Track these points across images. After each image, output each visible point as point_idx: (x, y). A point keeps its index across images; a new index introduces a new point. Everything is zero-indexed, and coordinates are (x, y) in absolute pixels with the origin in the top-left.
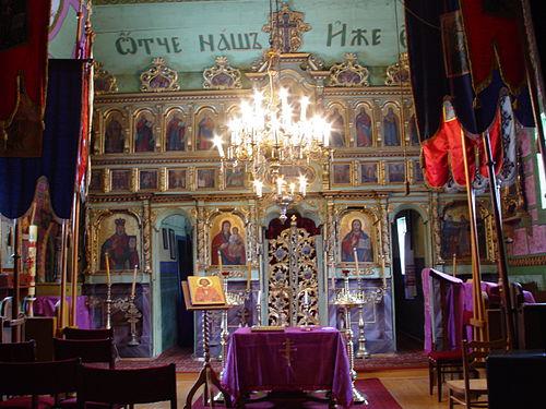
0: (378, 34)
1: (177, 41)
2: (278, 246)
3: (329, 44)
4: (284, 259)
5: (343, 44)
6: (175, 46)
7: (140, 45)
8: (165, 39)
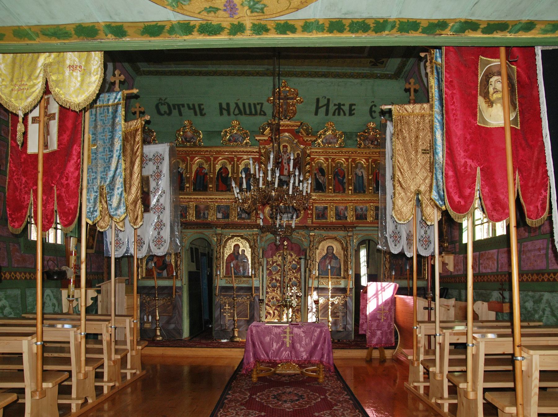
0: (353, 107)
1: (202, 107)
2: (273, 263)
3: (316, 113)
4: (278, 272)
5: (327, 114)
6: (201, 110)
7: (175, 109)
8: (194, 105)
